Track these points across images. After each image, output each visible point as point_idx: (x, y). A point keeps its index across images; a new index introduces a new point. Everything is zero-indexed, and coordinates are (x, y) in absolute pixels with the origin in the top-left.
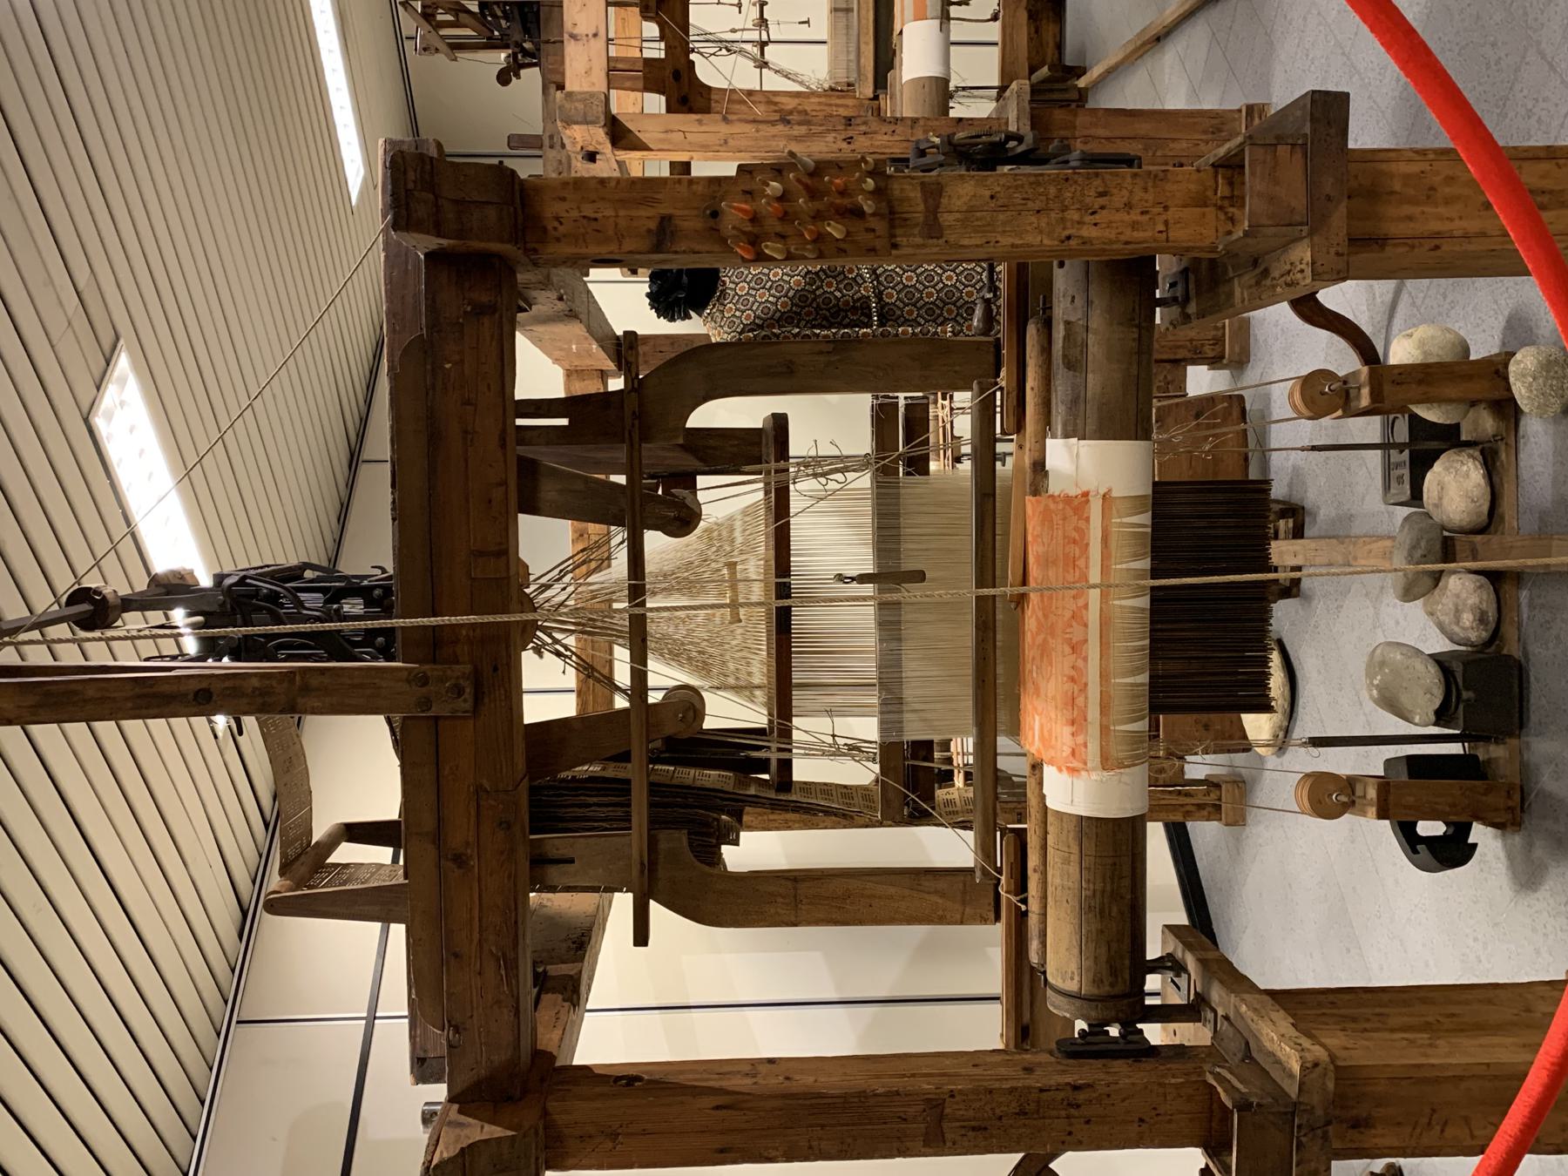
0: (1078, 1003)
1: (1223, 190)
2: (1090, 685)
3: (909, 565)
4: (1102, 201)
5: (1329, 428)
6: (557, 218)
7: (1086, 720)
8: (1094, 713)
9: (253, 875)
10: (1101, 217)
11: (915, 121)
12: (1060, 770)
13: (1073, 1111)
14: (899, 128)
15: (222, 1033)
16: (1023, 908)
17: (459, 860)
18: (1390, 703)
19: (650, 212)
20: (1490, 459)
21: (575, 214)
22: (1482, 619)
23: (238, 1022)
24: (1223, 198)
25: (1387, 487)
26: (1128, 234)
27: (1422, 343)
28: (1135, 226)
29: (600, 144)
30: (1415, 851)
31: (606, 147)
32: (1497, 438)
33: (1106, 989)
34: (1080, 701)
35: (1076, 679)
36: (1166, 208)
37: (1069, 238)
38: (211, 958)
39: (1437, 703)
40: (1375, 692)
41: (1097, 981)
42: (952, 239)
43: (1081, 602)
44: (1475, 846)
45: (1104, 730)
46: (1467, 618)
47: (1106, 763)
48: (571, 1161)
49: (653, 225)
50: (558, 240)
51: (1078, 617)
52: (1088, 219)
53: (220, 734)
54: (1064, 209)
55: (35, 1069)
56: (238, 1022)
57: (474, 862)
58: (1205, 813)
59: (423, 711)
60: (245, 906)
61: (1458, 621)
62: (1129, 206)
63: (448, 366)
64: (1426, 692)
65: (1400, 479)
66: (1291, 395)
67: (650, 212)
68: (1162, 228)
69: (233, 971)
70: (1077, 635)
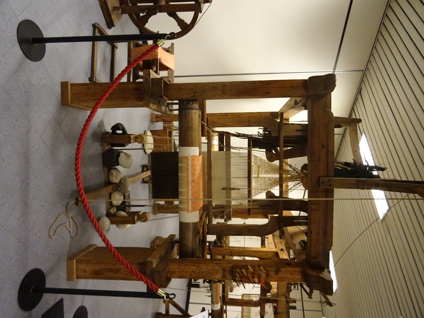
0: (192, 108)
1: (169, 274)
2: (191, 174)
3: (225, 191)
4: (192, 273)
5: (142, 210)
6: (298, 275)
7: (191, 167)
8: (190, 168)
9: (357, 101)
10: (192, 270)
11: (218, 255)
12: (196, 156)
13: (195, 91)
14: (221, 253)
15: (367, 68)
16: (202, 122)
17: (323, 146)
18: (128, 156)
19: (280, 276)
20: (111, 204)
21: (295, 276)
22: (112, 174)
23: (363, 71)
24: (169, 273)
25: (129, 194)
26: (186, 267)
27: (125, 227)
28: (185, 268)
29: (281, 253)
30: (123, 128)
31: (279, 252)
32: (110, 209)
33: (187, 111)
34: (193, 170)
35: (193, 174)
36: (179, 271)
37: (198, 267)
38: (369, 87)
39: (120, 158)
40: (131, 158)
41: (189, 113)
42: (221, 268)
43: (193, 190)
44: (111, 129)
45: (188, 165)
46: (115, 174)
47: (187, 158)
48: (302, 81)
49: (279, 273)
50: (298, 271)
51: (193, 187)
52: (194, 270)
53: (364, 133)
54: (199, 272)
55: (418, 102)
56: (363, 71)
57: (320, 146)
58: (159, 116)
59: (330, 179)
60: (360, 94)
61: (116, 174)
62: (186, 272)
63: (322, 247)
64: (122, 158)
65: (127, 196)
66: (149, 217)
67: (280, 276)
68: (180, 268)
69: (364, 81)
70: (193, 184)
